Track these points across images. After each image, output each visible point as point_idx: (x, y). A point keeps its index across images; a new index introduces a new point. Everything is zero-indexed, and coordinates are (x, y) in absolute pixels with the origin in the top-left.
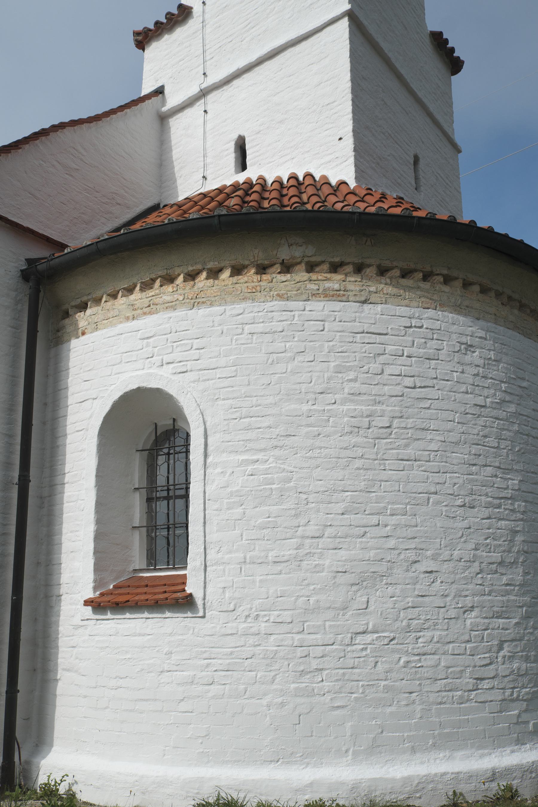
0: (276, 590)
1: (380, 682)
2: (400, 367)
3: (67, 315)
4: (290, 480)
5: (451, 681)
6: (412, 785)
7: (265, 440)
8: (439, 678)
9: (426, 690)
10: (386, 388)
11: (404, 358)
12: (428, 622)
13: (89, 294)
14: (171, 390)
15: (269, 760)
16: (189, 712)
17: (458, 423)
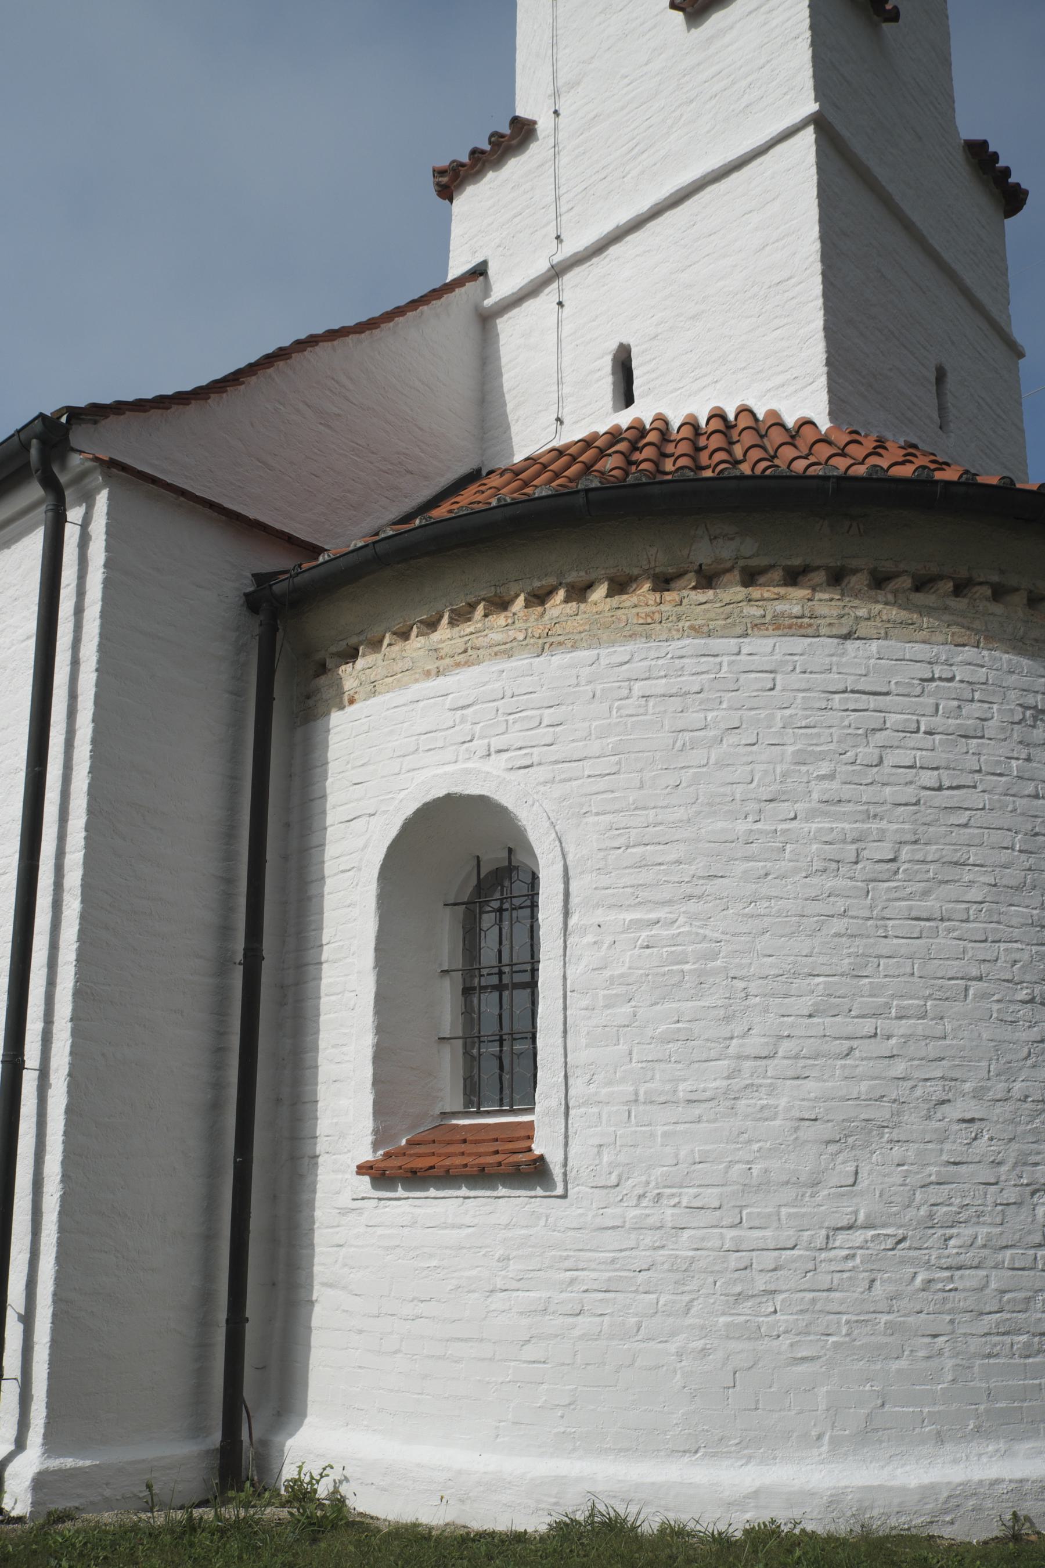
0: (692, 1151)
1: (879, 1316)
2: (914, 752)
3: (322, 669)
4: (715, 956)
5: (1008, 1316)
6: (936, 1500)
7: (670, 885)
8: (988, 1310)
9: (964, 1331)
10: (888, 790)
11: (921, 735)
12: (967, 1210)
13: (361, 633)
14: (506, 799)
15: (681, 1449)
16: (540, 1362)
17: (1021, 851)
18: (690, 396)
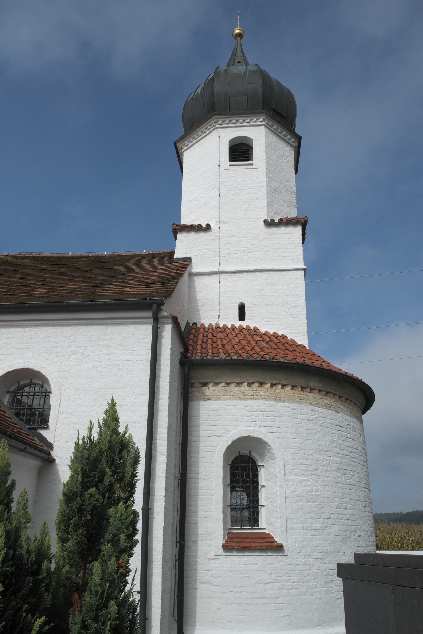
4: (318, 491)
18: (265, 325)
